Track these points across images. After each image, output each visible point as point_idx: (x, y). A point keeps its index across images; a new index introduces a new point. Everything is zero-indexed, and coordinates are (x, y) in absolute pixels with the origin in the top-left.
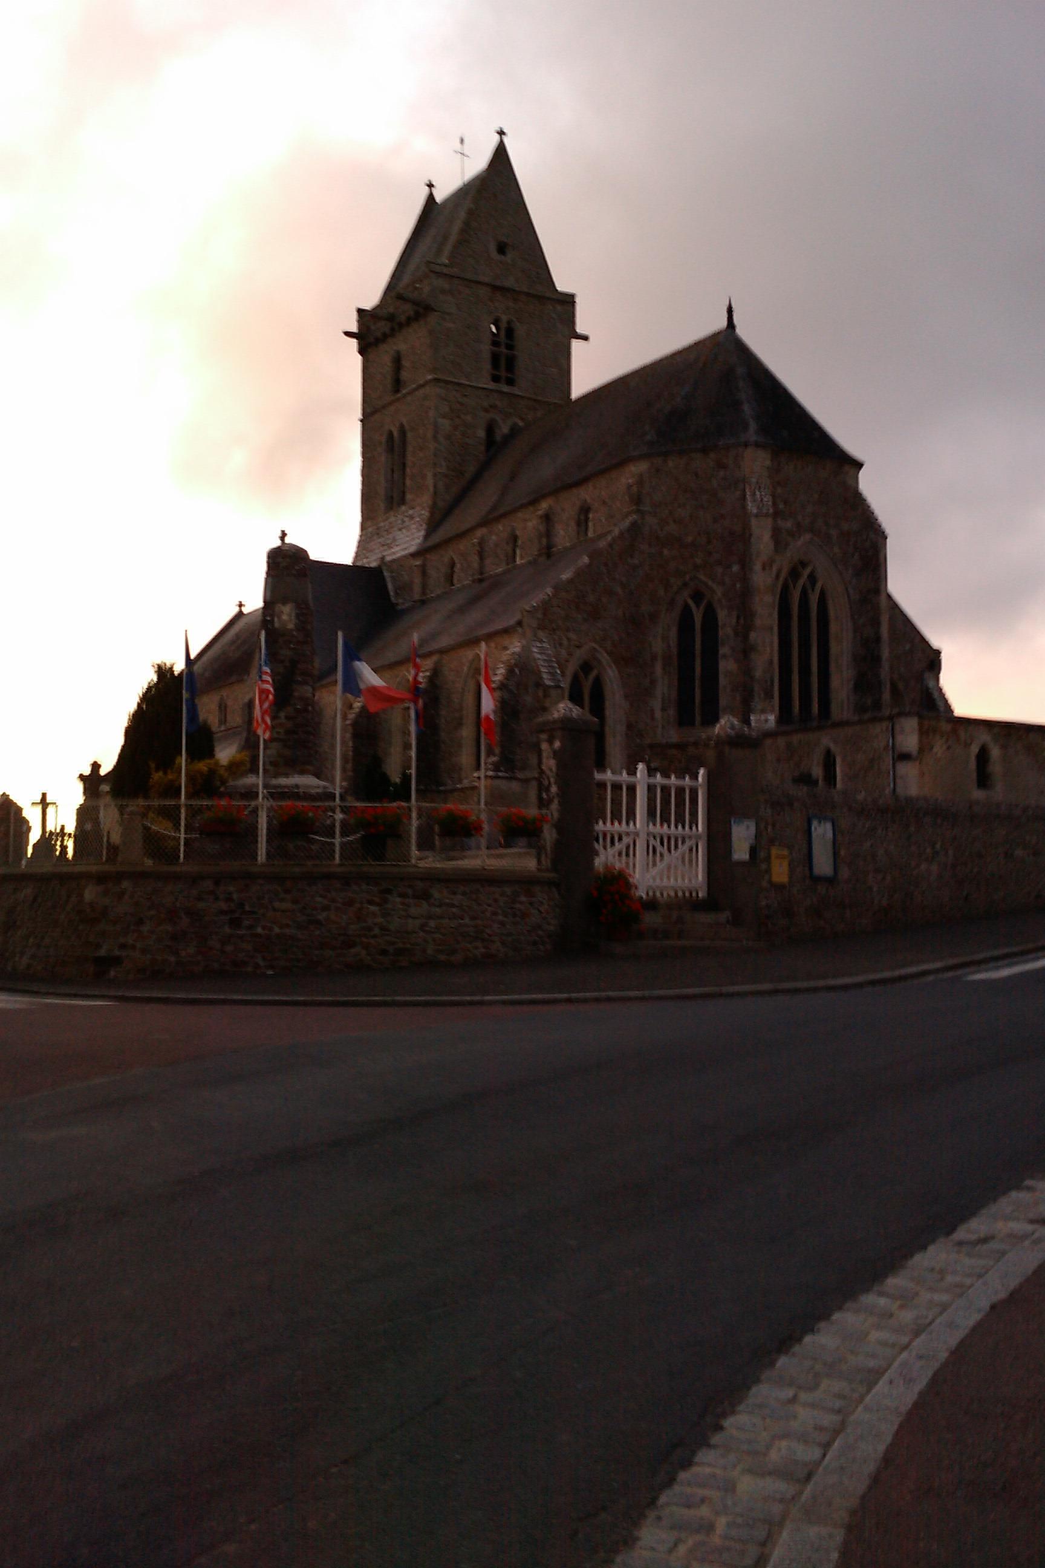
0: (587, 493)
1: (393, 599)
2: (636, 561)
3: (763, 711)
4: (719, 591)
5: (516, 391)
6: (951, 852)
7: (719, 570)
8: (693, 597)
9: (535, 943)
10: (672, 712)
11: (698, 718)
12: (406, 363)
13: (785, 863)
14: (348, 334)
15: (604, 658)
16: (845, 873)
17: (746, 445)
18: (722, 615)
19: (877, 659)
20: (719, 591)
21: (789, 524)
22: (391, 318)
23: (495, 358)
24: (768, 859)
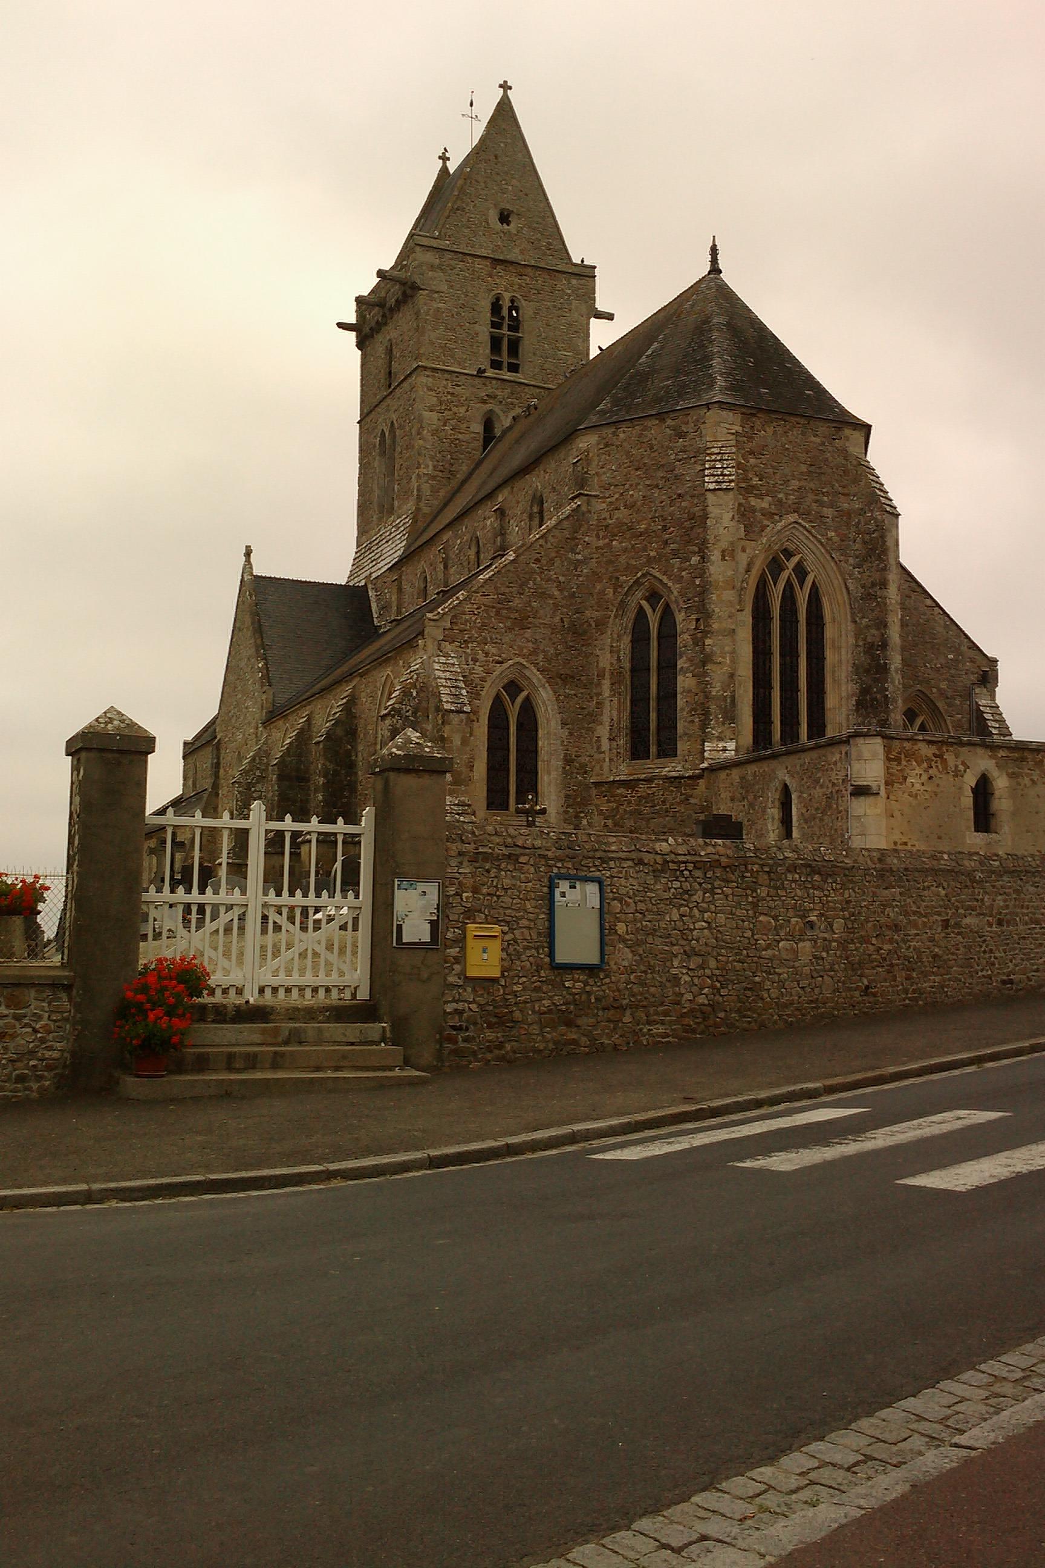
0: (536, 481)
2: (579, 557)
3: (720, 739)
4: (675, 588)
6: (838, 924)
8: (647, 599)
9: (21, 1079)
11: (653, 749)
12: (396, 353)
13: (495, 947)
14: (341, 325)
15: (535, 675)
16: (623, 957)
17: (708, 406)
19: (884, 669)
20: (675, 588)
21: (765, 503)
22: (381, 304)
23: (495, 343)
24: (461, 941)
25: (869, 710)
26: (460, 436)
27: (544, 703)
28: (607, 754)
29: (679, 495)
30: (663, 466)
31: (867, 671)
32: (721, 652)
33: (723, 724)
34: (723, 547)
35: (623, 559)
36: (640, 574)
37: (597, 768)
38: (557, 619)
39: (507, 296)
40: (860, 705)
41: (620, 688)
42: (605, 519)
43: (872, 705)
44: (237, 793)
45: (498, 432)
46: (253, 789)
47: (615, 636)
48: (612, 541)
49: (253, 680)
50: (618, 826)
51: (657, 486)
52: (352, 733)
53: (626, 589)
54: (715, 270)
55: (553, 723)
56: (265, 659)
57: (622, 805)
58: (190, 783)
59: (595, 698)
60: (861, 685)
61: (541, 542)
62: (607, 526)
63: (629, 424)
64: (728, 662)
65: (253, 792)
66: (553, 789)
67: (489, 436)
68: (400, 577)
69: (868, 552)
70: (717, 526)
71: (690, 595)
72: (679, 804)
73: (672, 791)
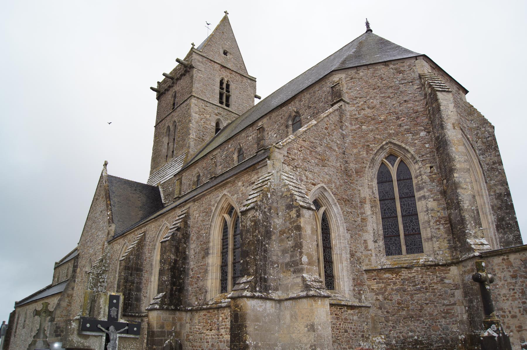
1: (163, 201)
5: (230, 109)
7: (410, 136)
10: (381, 243)
11: (404, 248)
18: (414, 169)
22: (172, 78)
25: (506, 230)
26: (207, 126)
27: (335, 215)
28: (373, 251)
29: (405, 101)
30: (391, 87)
31: (500, 208)
32: (465, 182)
33: (476, 227)
34: (453, 122)
35: (371, 136)
36: (384, 143)
37: (367, 261)
38: (338, 164)
39: (226, 79)
40: (498, 227)
41: (376, 210)
42: (355, 115)
43: (507, 227)
44: (91, 278)
45: (221, 127)
46: (100, 277)
47: (370, 179)
48: (362, 126)
49: (103, 222)
50: (388, 300)
51: (389, 97)
52: (186, 237)
53: (375, 151)
54: (369, 31)
55: (341, 229)
56: (111, 210)
57: (389, 285)
58: (56, 279)
59: (360, 216)
60: (498, 216)
61: (327, 118)
62: (357, 119)
63: (365, 68)
64: (470, 187)
65: (100, 279)
66: (345, 273)
67: (217, 129)
68: (182, 178)
69: (487, 147)
70: (447, 110)
71: (423, 154)
72: (436, 283)
73: (429, 275)
